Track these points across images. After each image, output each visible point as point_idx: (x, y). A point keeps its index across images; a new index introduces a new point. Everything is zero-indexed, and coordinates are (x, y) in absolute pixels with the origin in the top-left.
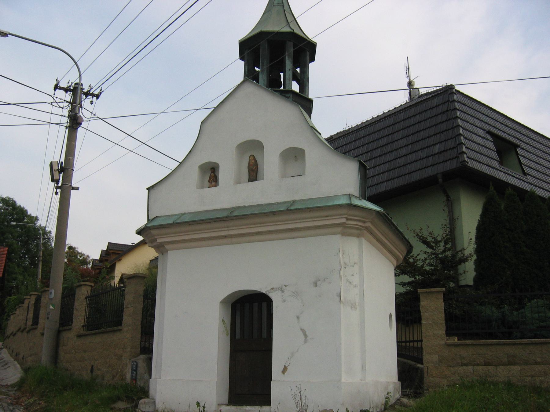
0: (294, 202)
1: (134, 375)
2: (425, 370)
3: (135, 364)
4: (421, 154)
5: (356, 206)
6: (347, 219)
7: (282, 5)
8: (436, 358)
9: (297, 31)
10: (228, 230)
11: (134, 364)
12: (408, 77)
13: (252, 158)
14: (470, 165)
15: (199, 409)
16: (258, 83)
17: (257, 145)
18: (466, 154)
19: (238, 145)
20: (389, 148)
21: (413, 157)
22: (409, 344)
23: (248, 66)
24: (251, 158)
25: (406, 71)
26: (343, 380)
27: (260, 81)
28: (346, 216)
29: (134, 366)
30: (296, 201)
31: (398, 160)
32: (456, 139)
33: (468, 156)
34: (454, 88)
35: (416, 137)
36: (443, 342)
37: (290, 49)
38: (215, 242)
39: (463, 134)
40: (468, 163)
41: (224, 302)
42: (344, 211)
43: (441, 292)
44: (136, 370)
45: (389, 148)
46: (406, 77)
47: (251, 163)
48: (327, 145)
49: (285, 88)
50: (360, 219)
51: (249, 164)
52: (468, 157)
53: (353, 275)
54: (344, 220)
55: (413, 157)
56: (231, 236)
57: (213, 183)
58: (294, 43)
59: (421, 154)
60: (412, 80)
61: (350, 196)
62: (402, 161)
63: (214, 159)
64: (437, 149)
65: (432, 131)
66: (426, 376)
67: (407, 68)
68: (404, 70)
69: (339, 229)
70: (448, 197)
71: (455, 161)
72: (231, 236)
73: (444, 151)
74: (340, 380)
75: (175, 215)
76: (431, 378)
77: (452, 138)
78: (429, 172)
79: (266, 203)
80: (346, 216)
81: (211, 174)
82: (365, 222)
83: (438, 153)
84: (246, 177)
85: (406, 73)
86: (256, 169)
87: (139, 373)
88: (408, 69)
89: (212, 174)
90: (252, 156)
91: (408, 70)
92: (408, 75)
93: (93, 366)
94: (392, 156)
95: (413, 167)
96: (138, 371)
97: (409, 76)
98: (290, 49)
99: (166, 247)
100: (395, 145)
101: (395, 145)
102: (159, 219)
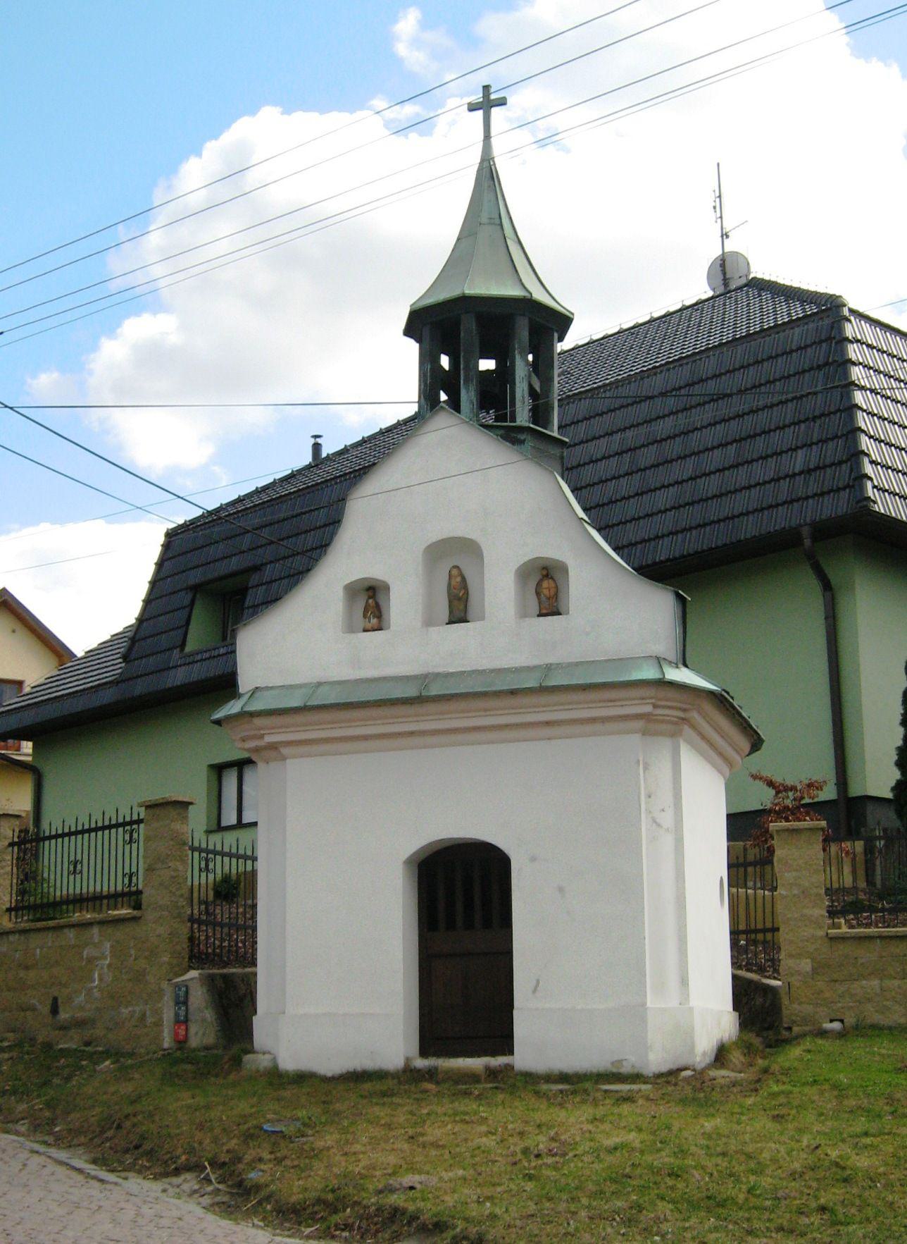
0: (549, 667)
1: (182, 1013)
2: (783, 994)
3: (184, 989)
4: (760, 472)
5: (672, 684)
6: (655, 706)
7: (497, 221)
8: (806, 965)
9: (539, 295)
10: (418, 721)
11: (180, 989)
12: (719, 220)
13: (455, 572)
14: (880, 508)
15: (27, 1159)
16: (459, 413)
17: (470, 548)
18: (871, 479)
19: (429, 547)
20: (676, 447)
21: (741, 476)
22: (773, 936)
23: (431, 363)
24: (453, 572)
25: (714, 204)
26: (649, 1004)
27: (462, 407)
28: (653, 701)
29: (182, 994)
30: (553, 667)
31: (700, 481)
32: (847, 439)
33: (876, 484)
34: (845, 306)
35: (748, 424)
36: (821, 933)
37: (523, 333)
38: (386, 743)
39: (866, 429)
40: (875, 502)
41: (408, 862)
42: (650, 692)
43: (818, 829)
44: (185, 1003)
45: (676, 447)
46: (714, 219)
47: (453, 583)
48: (620, 564)
49: (515, 422)
50: (675, 704)
51: (449, 584)
52: (874, 487)
53: (663, 810)
54: (649, 709)
55: (741, 476)
56: (423, 733)
57: (374, 621)
58: (530, 318)
59: (760, 472)
60: (727, 230)
61: (659, 661)
62: (711, 485)
63: (374, 570)
64: (799, 460)
65: (789, 413)
66: (785, 1001)
67: (718, 195)
68: (710, 200)
69: (640, 724)
70: (827, 586)
71: (845, 495)
72: (423, 733)
73: (817, 468)
74: (644, 1004)
75: (300, 686)
76: (795, 1006)
77: (836, 437)
78: (780, 520)
79: (492, 668)
80: (653, 701)
81: (367, 601)
82: (685, 710)
83: (801, 473)
84: (443, 610)
85: (715, 208)
86: (465, 596)
87: (191, 1008)
88: (720, 197)
89: (370, 601)
90: (457, 567)
91: (718, 200)
92: (719, 215)
93: (55, 999)
94: (688, 468)
95: (740, 502)
96: (189, 1003)
97: (721, 217)
98: (523, 333)
99: (285, 751)
100: (695, 441)
101: (695, 441)
102: (266, 693)
